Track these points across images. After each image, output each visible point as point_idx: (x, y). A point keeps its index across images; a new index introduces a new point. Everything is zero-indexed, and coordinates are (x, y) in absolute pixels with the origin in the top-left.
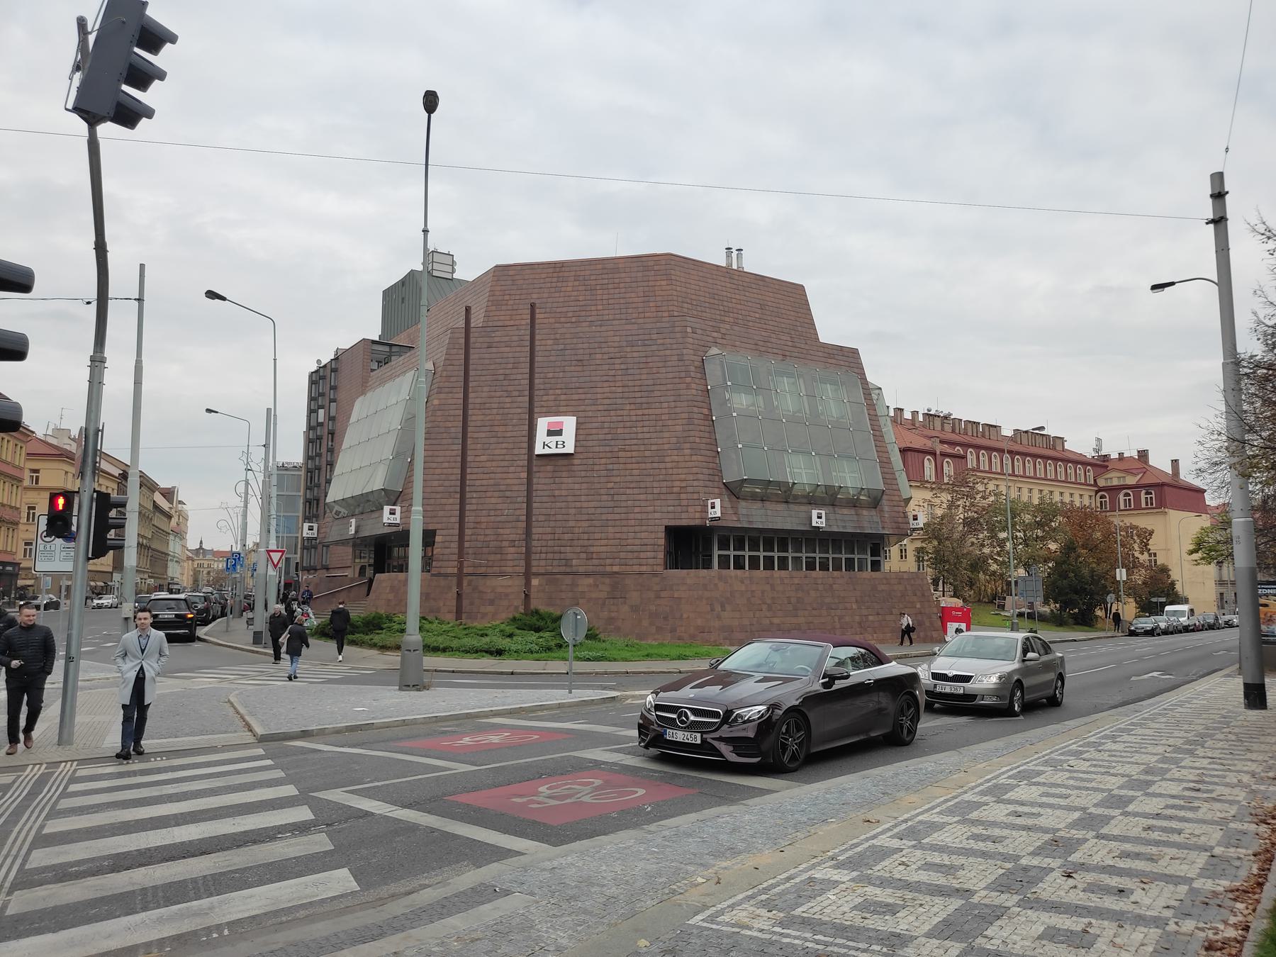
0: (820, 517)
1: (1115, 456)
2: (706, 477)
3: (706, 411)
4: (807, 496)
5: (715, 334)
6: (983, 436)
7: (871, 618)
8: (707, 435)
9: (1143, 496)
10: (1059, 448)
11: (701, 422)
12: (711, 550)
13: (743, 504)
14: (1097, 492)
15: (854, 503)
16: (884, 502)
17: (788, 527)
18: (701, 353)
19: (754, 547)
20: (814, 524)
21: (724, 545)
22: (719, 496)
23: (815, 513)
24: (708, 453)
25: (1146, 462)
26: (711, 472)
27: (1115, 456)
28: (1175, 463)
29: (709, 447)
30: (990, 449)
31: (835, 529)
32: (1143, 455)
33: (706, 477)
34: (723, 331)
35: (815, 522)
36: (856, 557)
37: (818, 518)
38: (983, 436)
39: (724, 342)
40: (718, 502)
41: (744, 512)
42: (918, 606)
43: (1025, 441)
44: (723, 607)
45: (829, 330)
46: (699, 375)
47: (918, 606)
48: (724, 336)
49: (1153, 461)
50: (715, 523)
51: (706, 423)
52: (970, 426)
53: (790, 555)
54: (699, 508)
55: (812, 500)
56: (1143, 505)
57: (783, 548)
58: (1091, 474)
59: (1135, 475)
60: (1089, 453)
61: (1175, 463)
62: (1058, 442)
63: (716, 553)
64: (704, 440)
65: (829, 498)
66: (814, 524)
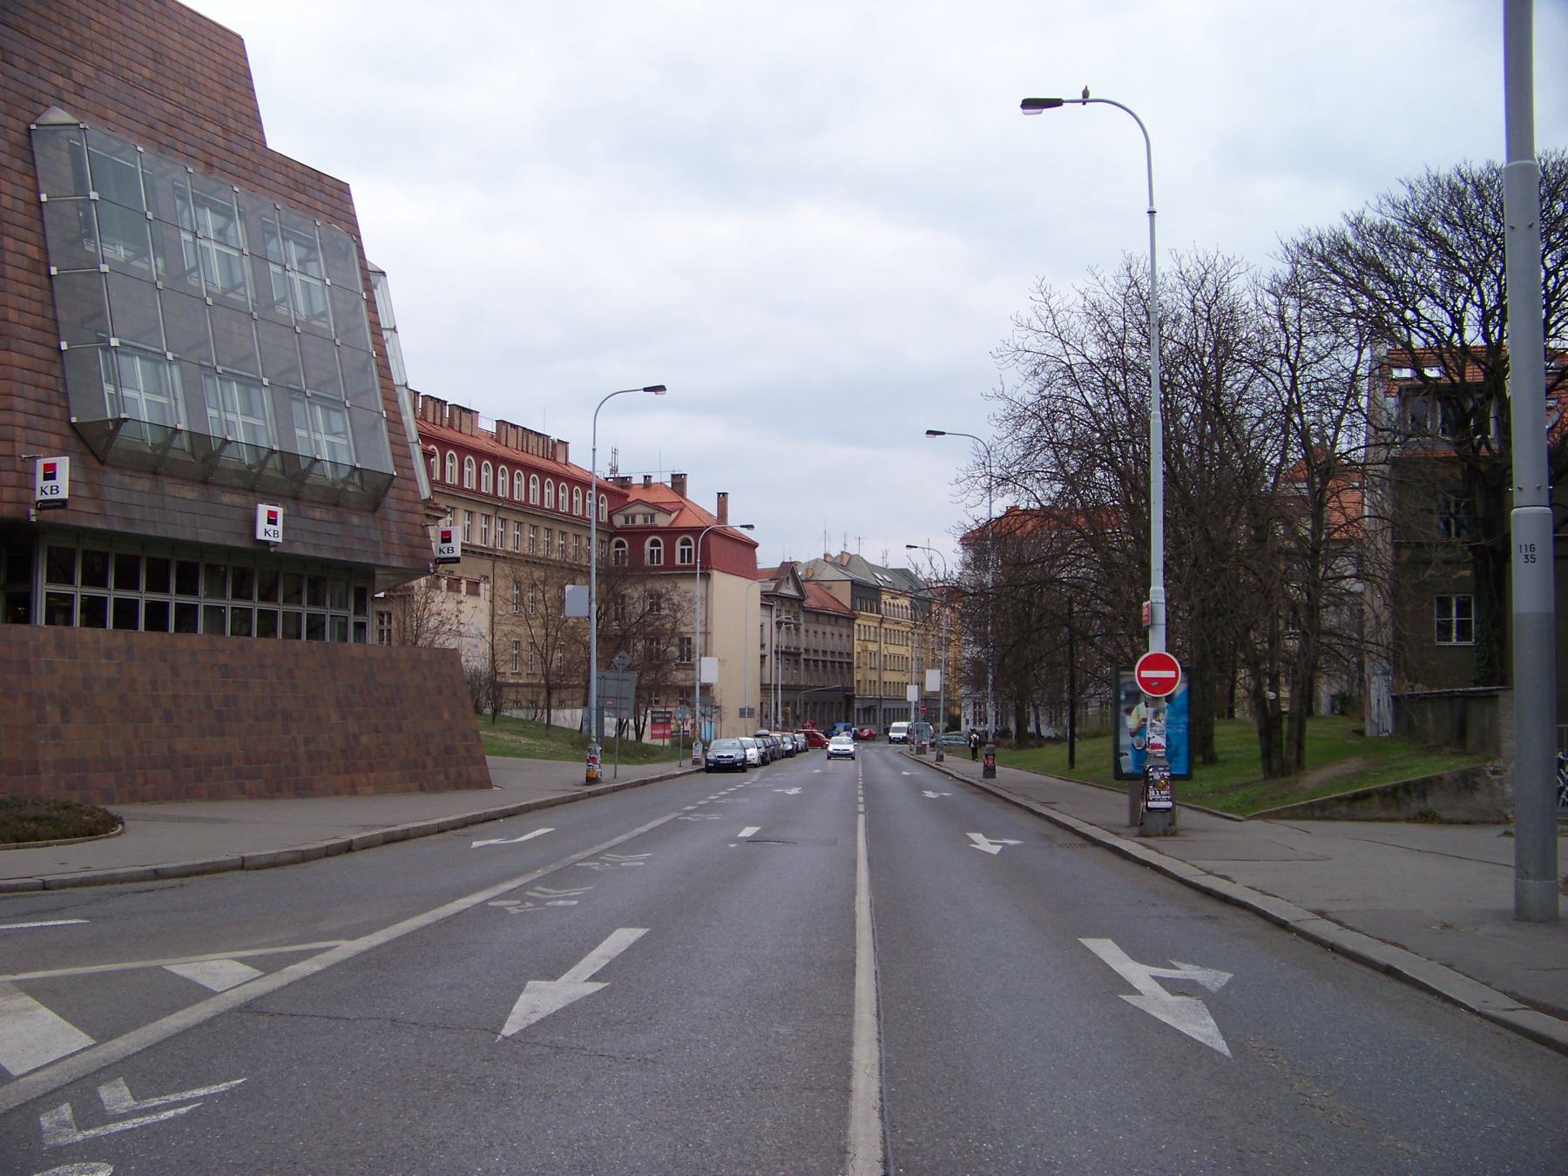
0: (272, 521)
1: (638, 480)
2: (32, 407)
3: (33, 251)
4: (244, 473)
5: (59, 80)
6: (451, 426)
7: (364, 740)
8: (36, 307)
9: (678, 547)
10: (561, 459)
11: (22, 275)
12: (28, 577)
13: (115, 477)
14: (612, 536)
15: (334, 498)
16: (390, 502)
17: (206, 537)
18: (27, 116)
19: (127, 580)
20: (260, 536)
21: (61, 574)
22: (63, 452)
23: (263, 510)
24: (40, 351)
25: (682, 493)
26: (42, 394)
27: (638, 480)
28: (722, 497)
29: (39, 336)
30: (462, 450)
31: (299, 550)
32: (679, 482)
33: (32, 407)
34: (80, 78)
35: (264, 532)
36: (328, 612)
37: (270, 525)
38: (451, 426)
39: (81, 102)
40: (63, 464)
41: (114, 495)
42: (446, 716)
43: (512, 443)
44: (66, 716)
45: (287, 133)
46: (18, 164)
47: (446, 716)
48: (80, 90)
49: (693, 492)
50: (49, 515)
51: (35, 279)
52: (430, 404)
53: (201, 601)
54: (12, 478)
55: (255, 484)
56: (678, 561)
57: (188, 585)
58: (604, 506)
59: (670, 513)
60: (603, 472)
61: (722, 497)
62: (560, 448)
63: (43, 588)
64: (28, 319)
65: (288, 478)
66: (260, 536)
